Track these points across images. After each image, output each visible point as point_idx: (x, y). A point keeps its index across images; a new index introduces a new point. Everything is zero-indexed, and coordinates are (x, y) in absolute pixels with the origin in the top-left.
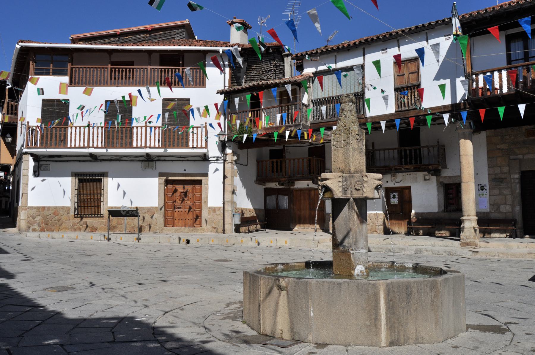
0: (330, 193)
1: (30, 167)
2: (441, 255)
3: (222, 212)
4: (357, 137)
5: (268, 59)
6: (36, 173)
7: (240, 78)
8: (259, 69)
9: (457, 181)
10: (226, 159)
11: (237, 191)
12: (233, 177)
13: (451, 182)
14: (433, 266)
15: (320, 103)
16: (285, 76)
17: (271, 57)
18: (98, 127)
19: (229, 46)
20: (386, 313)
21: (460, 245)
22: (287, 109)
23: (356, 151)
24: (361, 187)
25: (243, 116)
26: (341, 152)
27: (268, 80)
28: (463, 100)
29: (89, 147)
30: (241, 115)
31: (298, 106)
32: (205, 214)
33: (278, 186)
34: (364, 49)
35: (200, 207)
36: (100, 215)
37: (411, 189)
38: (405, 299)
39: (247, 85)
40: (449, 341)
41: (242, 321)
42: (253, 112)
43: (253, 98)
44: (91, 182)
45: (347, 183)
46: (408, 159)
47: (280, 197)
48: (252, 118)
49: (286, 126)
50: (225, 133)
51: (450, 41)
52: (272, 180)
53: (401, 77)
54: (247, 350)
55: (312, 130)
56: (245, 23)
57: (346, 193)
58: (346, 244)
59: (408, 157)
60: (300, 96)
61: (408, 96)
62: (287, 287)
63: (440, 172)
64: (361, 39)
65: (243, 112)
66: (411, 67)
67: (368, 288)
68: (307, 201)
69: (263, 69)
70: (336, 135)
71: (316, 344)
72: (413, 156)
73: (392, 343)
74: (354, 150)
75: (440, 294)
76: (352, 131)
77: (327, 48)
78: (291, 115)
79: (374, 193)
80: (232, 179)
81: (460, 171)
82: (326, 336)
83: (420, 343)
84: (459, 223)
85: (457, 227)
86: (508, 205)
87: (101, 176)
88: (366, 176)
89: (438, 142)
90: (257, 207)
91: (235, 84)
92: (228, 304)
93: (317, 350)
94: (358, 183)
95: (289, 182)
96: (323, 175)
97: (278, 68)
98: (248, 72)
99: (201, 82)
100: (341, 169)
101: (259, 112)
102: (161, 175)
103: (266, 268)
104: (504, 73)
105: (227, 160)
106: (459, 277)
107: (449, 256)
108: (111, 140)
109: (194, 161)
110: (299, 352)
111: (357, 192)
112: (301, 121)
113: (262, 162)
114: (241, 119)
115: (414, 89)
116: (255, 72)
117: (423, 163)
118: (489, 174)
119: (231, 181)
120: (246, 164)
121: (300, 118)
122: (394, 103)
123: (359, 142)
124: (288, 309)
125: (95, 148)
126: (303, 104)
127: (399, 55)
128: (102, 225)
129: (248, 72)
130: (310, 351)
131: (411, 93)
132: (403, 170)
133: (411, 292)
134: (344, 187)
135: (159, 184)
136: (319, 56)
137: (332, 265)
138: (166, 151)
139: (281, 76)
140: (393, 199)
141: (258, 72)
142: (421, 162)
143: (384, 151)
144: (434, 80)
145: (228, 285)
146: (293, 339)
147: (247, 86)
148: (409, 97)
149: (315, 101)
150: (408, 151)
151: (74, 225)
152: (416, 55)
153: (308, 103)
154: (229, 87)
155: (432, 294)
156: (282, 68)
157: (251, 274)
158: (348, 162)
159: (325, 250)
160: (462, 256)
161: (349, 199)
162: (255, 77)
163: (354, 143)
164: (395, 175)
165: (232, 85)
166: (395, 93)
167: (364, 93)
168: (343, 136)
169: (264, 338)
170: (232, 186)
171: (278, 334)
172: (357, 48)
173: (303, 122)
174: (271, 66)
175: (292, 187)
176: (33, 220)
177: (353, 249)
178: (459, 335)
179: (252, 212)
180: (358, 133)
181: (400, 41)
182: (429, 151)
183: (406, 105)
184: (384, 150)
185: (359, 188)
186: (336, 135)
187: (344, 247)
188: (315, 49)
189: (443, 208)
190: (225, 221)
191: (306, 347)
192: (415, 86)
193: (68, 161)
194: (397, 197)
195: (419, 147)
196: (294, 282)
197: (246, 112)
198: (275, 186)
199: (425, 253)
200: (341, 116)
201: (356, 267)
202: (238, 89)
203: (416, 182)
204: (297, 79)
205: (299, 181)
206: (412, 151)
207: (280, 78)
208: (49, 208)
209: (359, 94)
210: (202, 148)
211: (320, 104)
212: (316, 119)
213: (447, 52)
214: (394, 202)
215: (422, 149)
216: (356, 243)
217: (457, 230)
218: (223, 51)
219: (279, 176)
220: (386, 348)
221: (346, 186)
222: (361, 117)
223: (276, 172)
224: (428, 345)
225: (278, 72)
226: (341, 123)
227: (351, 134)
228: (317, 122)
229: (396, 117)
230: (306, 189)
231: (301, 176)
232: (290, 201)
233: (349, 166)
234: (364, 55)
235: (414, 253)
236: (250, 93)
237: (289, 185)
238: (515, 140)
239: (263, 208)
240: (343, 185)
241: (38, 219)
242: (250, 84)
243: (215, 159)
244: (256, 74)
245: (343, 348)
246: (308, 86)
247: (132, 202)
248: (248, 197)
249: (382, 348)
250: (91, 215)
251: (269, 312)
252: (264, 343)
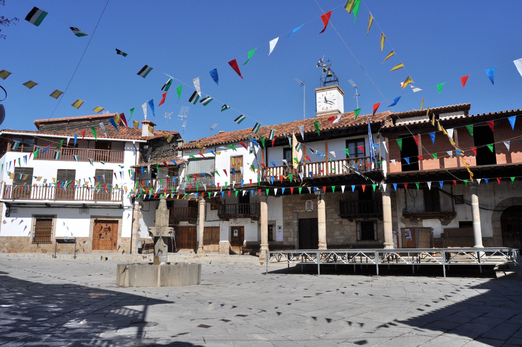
1: (3, 211)
4: (165, 213)
6: (8, 215)
12: (138, 219)
18: (52, 187)
29: (45, 199)
32: (119, 242)
35: (117, 237)
36: (50, 242)
44: (45, 221)
73: (162, 286)
87: (52, 217)
89: (256, 201)
99: (121, 160)
102: (92, 217)
104: (282, 168)
108: (60, 194)
109: (114, 208)
118: (283, 220)
120: (148, 210)
125: (49, 200)
128: (51, 249)
132: (238, 216)
135: (91, 223)
138: (96, 202)
142: (250, 213)
151: (32, 248)
161: (159, 237)
163: (164, 215)
175: (178, 225)
176: (3, 245)
193: (30, 207)
194: (237, 232)
203: (247, 223)
208: (15, 237)
210: (118, 201)
241: (7, 244)
243: (127, 207)
247: (72, 234)
250: (44, 242)
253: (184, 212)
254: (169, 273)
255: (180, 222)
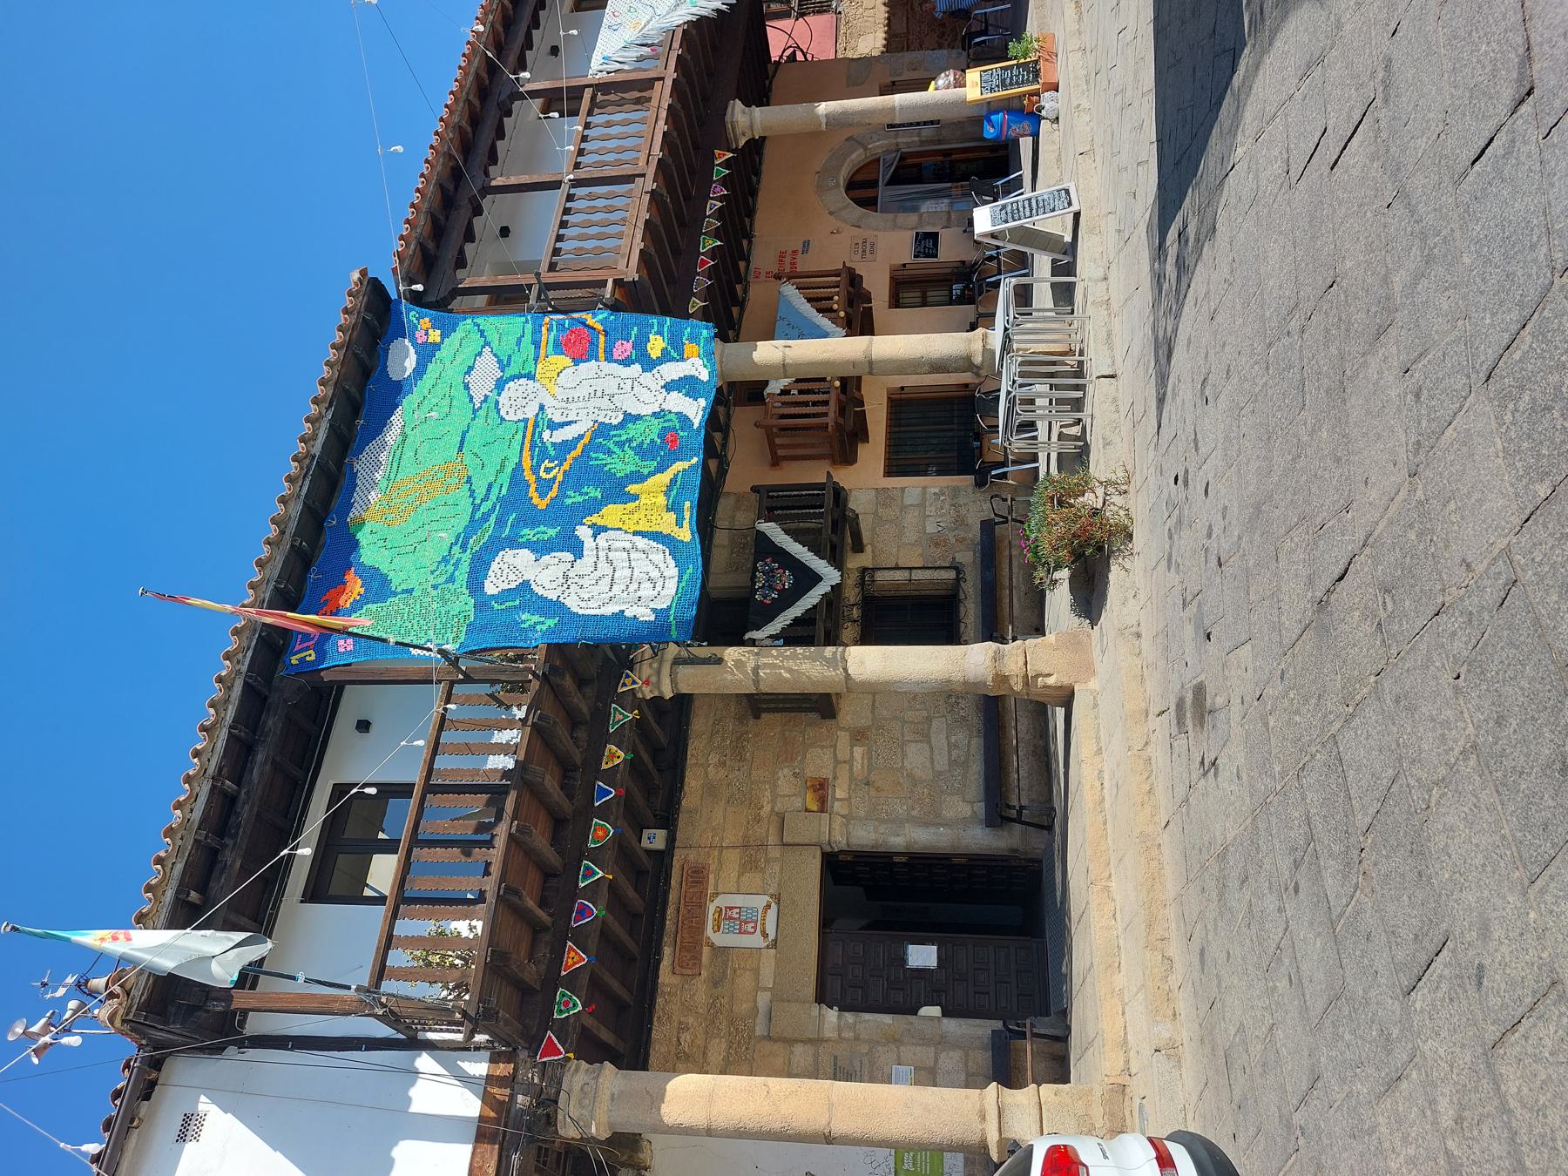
37: (810, 1077)
86: (936, 1061)
238: (701, 1011)
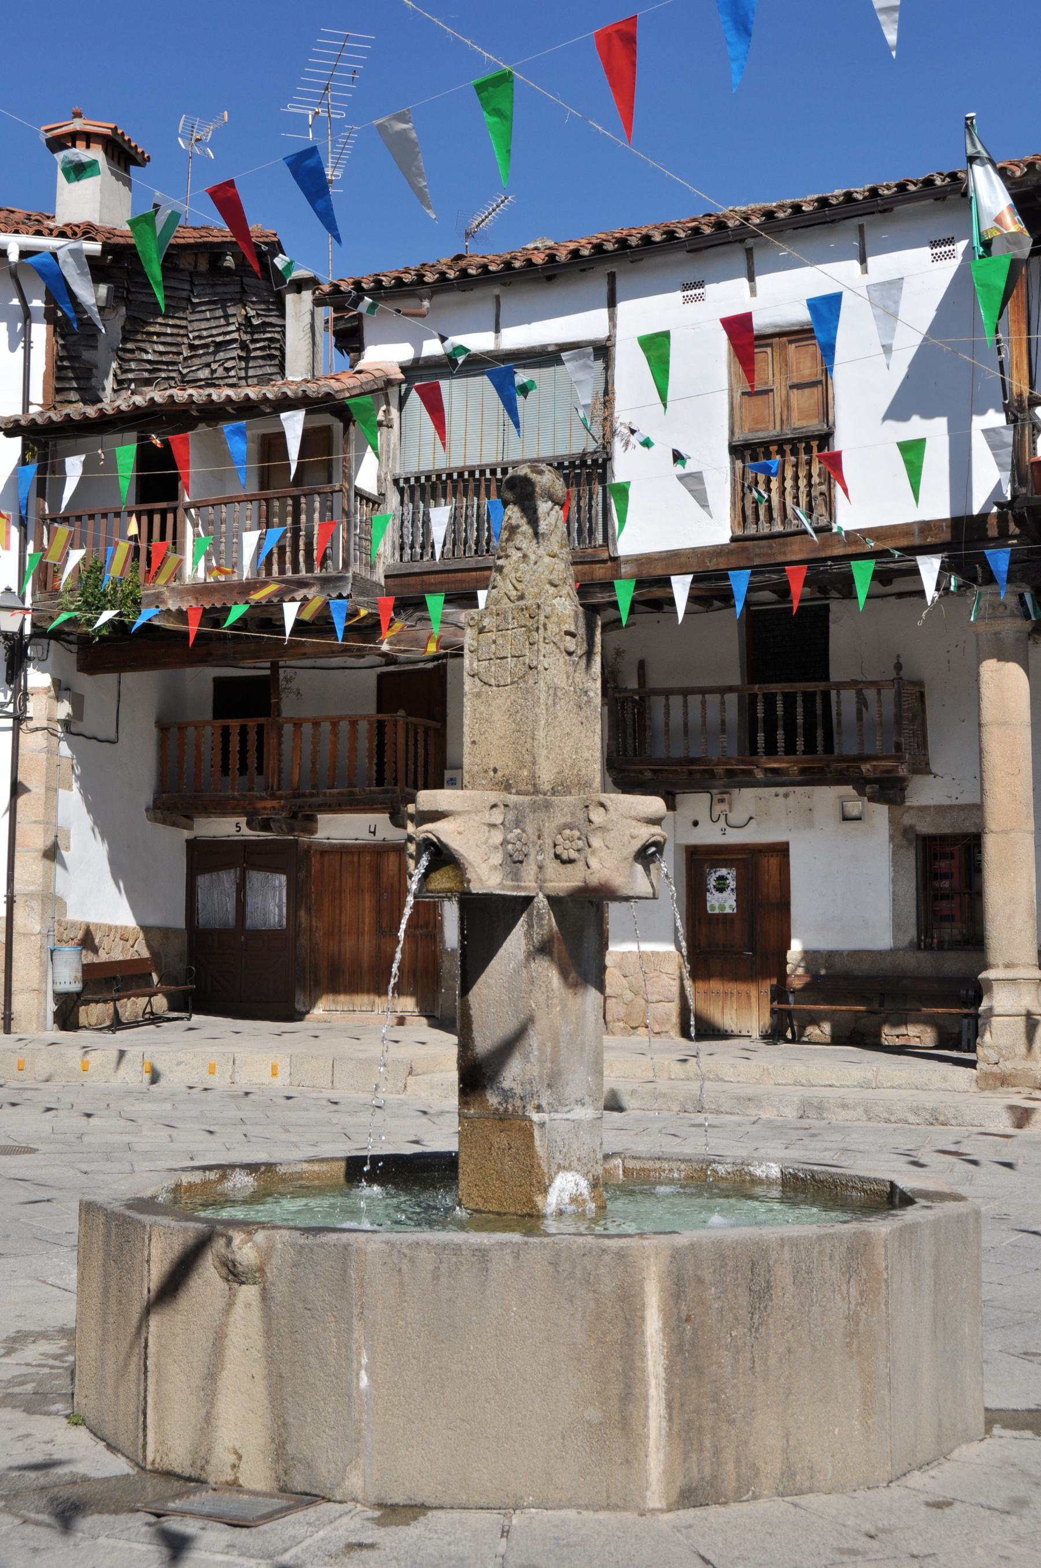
0: (451, 874)
2: (899, 1125)
3: (4, 940)
5: (215, 294)
7: (95, 371)
8: (178, 335)
9: (968, 827)
10: (25, 711)
11: (68, 848)
12: (51, 790)
13: (945, 827)
14: (861, 1174)
15: (429, 489)
16: (287, 372)
17: (231, 289)
19: (51, 230)
20: (670, 1370)
21: (974, 1084)
22: (290, 508)
23: (563, 702)
24: (578, 850)
25: (103, 535)
26: (501, 701)
27: (214, 385)
28: (998, 504)
30: (97, 529)
31: (338, 501)
33: (245, 830)
34: (612, 278)
38: (743, 1312)
39: (124, 401)
40: (917, 1479)
41: (67, 1417)
42: (144, 519)
43: (146, 458)
45: (523, 831)
46: (780, 735)
47: (256, 878)
48: (143, 545)
49: (282, 582)
50: (23, 602)
51: (950, 268)
52: (220, 808)
53: (758, 400)
54: (86, 1544)
55: (391, 601)
56: (119, 139)
57: (516, 874)
58: (514, 1085)
59: (780, 723)
60: (344, 459)
61: (784, 479)
62: (261, 1270)
63: (903, 790)
64: (603, 236)
65: (105, 516)
66: (798, 363)
67: (597, 1267)
68: (367, 897)
69: (195, 338)
70: (481, 631)
71: (381, 1506)
72: (800, 720)
74: (555, 694)
75: (883, 1291)
76: (547, 617)
77: (463, 263)
78: (306, 536)
79: (632, 875)
80: (47, 799)
81: (982, 785)
82: (421, 1472)
83: (801, 1493)
84: (971, 993)
85: (966, 1011)
88: (602, 805)
89: (898, 667)
90: (154, 921)
91: (73, 396)
92: (14, 1340)
93: (383, 1532)
94: (567, 832)
95: (294, 816)
96: (427, 799)
97: (256, 336)
98: (129, 346)
100: (500, 774)
101: (170, 517)
103: (178, 1186)
105: (31, 718)
106: (960, 1219)
107: (931, 1128)
110: (304, 1544)
111: (561, 868)
112: (346, 564)
113: (182, 728)
114: (96, 544)
115: (808, 450)
116: (161, 348)
117: (836, 751)
119: (46, 809)
120: (112, 736)
121: (346, 550)
122: (728, 504)
123: (576, 665)
124: (263, 1362)
126: (356, 494)
127: (747, 318)
129: (129, 346)
130: (353, 1539)
131: (796, 466)
132: (760, 775)
133: (768, 1282)
134: (510, 847)
136: (430, 298)
137: (457, 1172)
139: (269, 370)
140: (717, 894)
141: (174, 349)
142: (829, 748)
143: (685, 696)
144: (885, 418)
145: (16, 1256)
146: (283, 1490)
147: (124, 408)
148: (789, 483)
149: (407, 480)
150: (779, 698)
152: (802, 315)
153: (379, 487)
154: (47, 406)
155: (853, 1291)
156: (277, 336)
157: (113, 1213)
158: (528, 746)
159: (435, 1105)
160: (982, 1130)
161: (528, 900)
162: (160, 370)
164: (725, 796)
165: (58, 398)
166: (733, 463)
167: (609, 459)
168: (512, 641)
169: (162, 1486)
170: (46, 831)
171: (219, 1470)
172: (583, 270)
173: (355, 568)
174: (228, 324)
175: (304, 839)
177: (544, 1104)
178: (955, 1454)
179: (131, 942)
180: (572, 629)
181: (757, 255)
182: (862, 702)
183: (775, 514)
184: (685, 692)
185: (573, 855)
186: (481, 631)
187: (507, 1095)
188: (415, 265)
189: (912, 933)
190: (14, 978)
191: (337, 1523)
192: (814, 437)
194: (732, 884)
195: (821, 686)
196: (293, 1245)
197: (118, 514)
198: (232, 830)
199: (839, 1116)
200: (507, 556)
201: (551, 1180)
202: (86, 418)
203: (810, 824)
204: (335, 385)
205: (335, 812)
206: (795, 702)
207: (264, 380)
209: (589, 462)
211: (428, 496)
212: (412, 559)
213: (937, 310)
214: (722, 907)
215: (833, 694)
216: (553, 1081)
217: (965, 1021)
218: (24, 254)
219: (251, 789)
220: (667, 1517)
221: (518, 844)
222: (594, 556)
223: (241, 774)
224: (832, 1497)
225: (258, 353)
226: (505, 585)
227: (545, 629)
228: (416, 568)
229: (734, 561)
230: (364, 846)
231: (344, 790)
232: (296, 896)
233: (534, 763)
234: (612, 304)
235: (795, 1114)
236: (134, 435)
237: (291, 830)
239: (180, 923)
240: (505, 842)
242: (138, 400)
244: (164, 359)
245: (490, 1519)
246: (380, 416)
248: (116, 875)
249: (648, 1515)
251: (183, 1378)
252: (157, 1507)
253: (353, 750)
254: (754, 1329)
255: (321, 817)
